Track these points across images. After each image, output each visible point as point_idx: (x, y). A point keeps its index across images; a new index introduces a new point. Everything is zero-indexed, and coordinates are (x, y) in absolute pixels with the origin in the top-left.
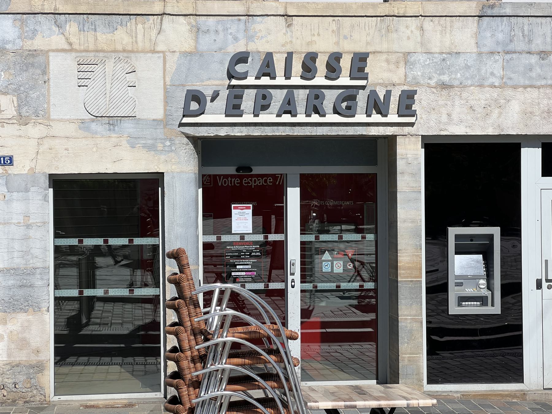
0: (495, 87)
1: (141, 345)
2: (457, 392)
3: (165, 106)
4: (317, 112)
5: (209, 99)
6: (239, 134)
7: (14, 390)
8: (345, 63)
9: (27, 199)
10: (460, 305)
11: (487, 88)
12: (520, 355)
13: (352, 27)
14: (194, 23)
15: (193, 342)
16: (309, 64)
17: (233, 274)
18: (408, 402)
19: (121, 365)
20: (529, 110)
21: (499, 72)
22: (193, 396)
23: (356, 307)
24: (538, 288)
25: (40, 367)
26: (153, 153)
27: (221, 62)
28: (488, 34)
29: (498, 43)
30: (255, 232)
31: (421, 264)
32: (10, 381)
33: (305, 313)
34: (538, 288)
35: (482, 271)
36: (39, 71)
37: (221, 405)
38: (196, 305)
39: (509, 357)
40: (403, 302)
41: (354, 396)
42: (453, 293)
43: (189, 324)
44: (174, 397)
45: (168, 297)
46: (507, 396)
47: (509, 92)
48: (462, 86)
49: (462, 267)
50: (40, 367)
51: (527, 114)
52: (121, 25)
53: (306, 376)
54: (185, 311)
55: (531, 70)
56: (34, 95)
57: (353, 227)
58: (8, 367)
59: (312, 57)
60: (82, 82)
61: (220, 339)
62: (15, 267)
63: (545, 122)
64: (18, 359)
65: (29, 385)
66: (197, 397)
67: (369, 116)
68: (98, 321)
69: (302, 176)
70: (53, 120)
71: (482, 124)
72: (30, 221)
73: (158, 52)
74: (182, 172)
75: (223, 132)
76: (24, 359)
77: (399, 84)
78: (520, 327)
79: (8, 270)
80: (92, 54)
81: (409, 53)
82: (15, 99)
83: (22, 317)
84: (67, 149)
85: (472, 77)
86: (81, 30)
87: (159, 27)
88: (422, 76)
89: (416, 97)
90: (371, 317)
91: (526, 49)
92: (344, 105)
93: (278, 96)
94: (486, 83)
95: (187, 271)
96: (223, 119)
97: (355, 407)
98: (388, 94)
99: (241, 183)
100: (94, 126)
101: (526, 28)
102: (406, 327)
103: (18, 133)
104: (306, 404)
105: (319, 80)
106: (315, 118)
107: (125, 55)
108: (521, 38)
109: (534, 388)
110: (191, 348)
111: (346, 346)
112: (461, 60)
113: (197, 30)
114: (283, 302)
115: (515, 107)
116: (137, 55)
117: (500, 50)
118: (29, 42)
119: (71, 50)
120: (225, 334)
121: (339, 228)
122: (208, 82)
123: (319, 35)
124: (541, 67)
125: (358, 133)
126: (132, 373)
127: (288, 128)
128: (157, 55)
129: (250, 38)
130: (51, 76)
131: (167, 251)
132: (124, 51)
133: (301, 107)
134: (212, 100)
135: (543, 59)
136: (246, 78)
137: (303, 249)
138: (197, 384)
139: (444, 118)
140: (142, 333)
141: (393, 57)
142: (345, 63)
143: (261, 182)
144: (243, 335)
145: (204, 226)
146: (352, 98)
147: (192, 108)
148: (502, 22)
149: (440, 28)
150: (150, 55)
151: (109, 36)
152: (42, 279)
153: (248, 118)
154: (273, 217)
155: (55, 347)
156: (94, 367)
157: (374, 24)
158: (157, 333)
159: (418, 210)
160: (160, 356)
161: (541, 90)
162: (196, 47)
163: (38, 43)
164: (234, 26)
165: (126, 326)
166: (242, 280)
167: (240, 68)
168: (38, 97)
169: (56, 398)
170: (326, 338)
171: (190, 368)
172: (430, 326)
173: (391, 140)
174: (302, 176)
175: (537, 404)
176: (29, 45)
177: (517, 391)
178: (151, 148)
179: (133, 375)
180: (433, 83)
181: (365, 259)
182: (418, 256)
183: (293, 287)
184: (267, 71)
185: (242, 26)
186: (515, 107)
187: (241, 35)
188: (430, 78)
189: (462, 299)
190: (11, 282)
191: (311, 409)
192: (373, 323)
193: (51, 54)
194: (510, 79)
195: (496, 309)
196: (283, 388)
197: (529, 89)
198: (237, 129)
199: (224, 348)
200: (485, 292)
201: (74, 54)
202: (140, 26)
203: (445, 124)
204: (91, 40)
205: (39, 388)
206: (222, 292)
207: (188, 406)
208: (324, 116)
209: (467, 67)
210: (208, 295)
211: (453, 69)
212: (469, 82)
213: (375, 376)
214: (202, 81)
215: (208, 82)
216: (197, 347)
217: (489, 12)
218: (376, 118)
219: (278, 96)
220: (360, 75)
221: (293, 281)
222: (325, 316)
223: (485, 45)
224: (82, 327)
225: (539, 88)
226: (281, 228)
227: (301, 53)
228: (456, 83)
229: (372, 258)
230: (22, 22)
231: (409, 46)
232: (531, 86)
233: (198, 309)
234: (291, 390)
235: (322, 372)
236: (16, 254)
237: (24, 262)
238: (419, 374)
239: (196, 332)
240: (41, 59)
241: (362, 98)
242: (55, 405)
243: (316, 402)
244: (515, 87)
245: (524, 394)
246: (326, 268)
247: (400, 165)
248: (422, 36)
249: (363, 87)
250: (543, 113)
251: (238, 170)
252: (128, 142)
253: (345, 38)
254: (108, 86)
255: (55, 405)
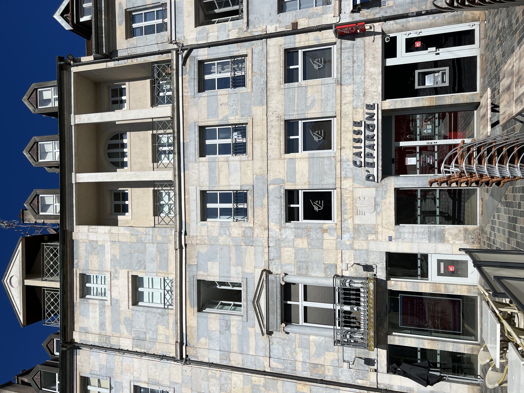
0: (365, 77)
1: (457, 195)
2: (480, 80)
3: (371, 188)
4: (373, 137)
5: (369, 173)
6: (381, 163)
7: (474, 239)
8: (356, 129)
9: (404, 233)
10: (445, 82)
11: (365, 80)
12: (464, 58)
13: (344, 127)
14: (343, 178)
15: (465, 177)
16: (357, 141)
17: (431, 164)
18: (489, 98)
19: (465, 202)
20: (373, 65)
21: (360, 76)
22: (486, 177)
23: (443, 119)
24: (439, 54)
25: (466, 230)
26: (387, 192)
27: (356, 169)
28: (347, 81)
29: (350, 78)
30: (416, 156)
31: (429, 97)
32: (471, 240)
33: (445, 138)
34: (439, 54)
35: (432, 75)
36: (360, 227)
37: (479, 167)
38: (450, 176)
39: (465, 62)
40: (443, 103)
41: (486, 118)
42: (440, 85)
43: (457, 179)
44: (466, 184)
45: (446, 186)
46: (482, 61)
47: (367, 72)
48: (365, 88)
49: (430, 83)
50: (466, 230)
51: (374, 65)
52: (344, 201)
53: (472, 136)
54: (453, 180)
55: (359, 66)
56: (368, 229)
57: (411, 123)
58: (465, 241)
59: (355, 140)
60: (363, 214)
61: (464, 168)
62: (428, 237)
63: (377, 59)
64: (462, 237)
65: (473, 234)
66: (487, 176)
67: (375, 120)
68: (447, 210)
69: (396, 141)
70: (376, 223)
71: (378, 80)
72: (411, 231)
73: (353, 190)
74: (394, 182)
75: (380, 168)
76: (462, 235)
77: (364, 110)
78: (453, 59)
79: (429, 239)
80: (354, 210)
81: (353, 108)
82: (369, 235)
83: (446, 235)
84: (386, 219)
85: (361, 85)
86: (346, 214)
87: (345, 190)
88: (361, 102)
89: (368, 104)
90: (447, 115)
91: (352, 68)
92: (371, 128)
93: (368, 150)
94: (363, 80)
95: (437, 180)
96: (376, 169)
97: (490, 118)
98: (367, 113)
99: (397, 162)
100: (378, 211)
101: (345, 69)
102: (453, 101)
103: (381, 234)
104: (489, 136)
105: (362, 137)
106: (375, 138)
107: (354, 200)
108: (348, 70)
109: (479, 51)
110: (467, 178)
111: (459, 122)
112: (356, 90)
113: (346, 177)
114: (440, 146)
115: (372, 70)
116: (354, 196)
117: (352, 77)
118: (351, 230)
119: (353, 217)
120: (462, 166)
121: (411, 128)
122: (363, 173)
123: (347, 138)
124: (358, 62)
125: (381, 123)
126: (468, 199)
127: (379, 147)
128: (354, 190)
129: (348, 160)
130: (361, 223)
131: (429, 186)
132: (353, 200)
133: (372, 143)
134: (369, 172)
135: (355, 62)
136: (362, 161)
137: (423, 140)
138: (481, 176)
139: (376, 94)
140: (452, 195)
141: (355, 113)
142: (356, 129)
143: (397, 155)
144: (462, 160)
145: (409, 174)
146: (368, 125)
147: (372, 179)
148: (343, 77)
149: (345, 98)
150: (354, 193)
151: (348, 205)
152: (433, 228)
153: (375, 160)
154: (406, 151)
155: (457, 225)
156: (465, 212)
157: (343, 120)
158: (452, 190)
159: (408, 100)
160: (461, 189)
161: (366, 61)
162: (352, 178)
163: (351, 227)
164: (344, 165)
165: (449, 201)
166: (434, 161)
167: (358, 163)
168: (369, 228)
169: (478, 225)
170: (456, 130)
171: (475, 178)
172: (452, 92)
173: (383, 111)
174: (396, 141)
175: (486, 49)
176: (351, 230)
177: (480, 58)
178: (386, 192)
179: (469, 198)
180: (363, 99)
181: (425, 117)
182: (426, 99)
183: (437, 143)
184: (359, 154)
185: (344, 163)
186: (372, 70)
187: (347, 163)
188: (362, 100)
189: (443, 81)
190: (434, 239)
191: (491, 134)
192: (450, 113)
193: (354, 223)
194: (362, 72)
195: (447, 69)
196: (484, 145)
197: (366, 66)
198: (379, 164)
199: (489, 167)
200: (440, 73)
201: (354, 216)
202: (345, 196)
203: (377, 93)
204: (349, 211)
205: (474, 230)
206: (445, 167)
207: (490, 179)
208: (375, 135)
209: (358, 87)
210: (446, 172)
211: (359, 92)
212: (363, 86)
213: (472, 111)
214: (363, 175)
215: (363, 173)
216: (467, 176)
217: (340, 82)
218: (375, 117)
219: (368, 150)
220: (360, 123)
221: (434, 143)
222: (447, 130)
223: (351, 82)
224: (449, 216)
225: (365, 62)
226: (414, 148)
227: (353, 144)
228: (363, 91)
229: (424, 115)
230: (344, 231)
231: (351, 108)
232: (365, 65)
233: (452, 176)
234: (485, 142)
235: (470, 130)
236: (423, 237)
237: (426, 234)
238: (472, 95)
239: (461, 176)
240: (356, 226)
241: (368, 122)
242: (481, 225)
243: (488, 132)
244: (365, 70)
245: (482, 55)
246: (430, 131)
247: (392, 107)
248: (347, 104)
249: (365, 122)
250: (374, 60)
251: (393, 163)
252: (384, 200)
253: (348, 129)
254: (364, 206)
255: (481, 225)
